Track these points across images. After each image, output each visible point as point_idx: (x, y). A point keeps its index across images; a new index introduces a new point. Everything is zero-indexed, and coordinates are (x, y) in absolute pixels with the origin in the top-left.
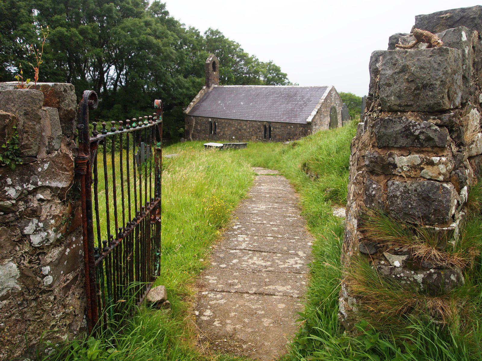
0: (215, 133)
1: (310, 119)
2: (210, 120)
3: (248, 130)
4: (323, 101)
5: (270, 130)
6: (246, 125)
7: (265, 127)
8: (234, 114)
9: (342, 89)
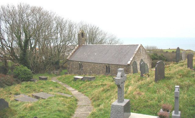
0: (82, 69)
1: (129, 63)
2: (80, 63)
3: (98, 68)
4: (136, 52)
5: (109, 68)
6: (97, 66)
7: (107, 66)
8: (91, 59)
9: (147, 44)
